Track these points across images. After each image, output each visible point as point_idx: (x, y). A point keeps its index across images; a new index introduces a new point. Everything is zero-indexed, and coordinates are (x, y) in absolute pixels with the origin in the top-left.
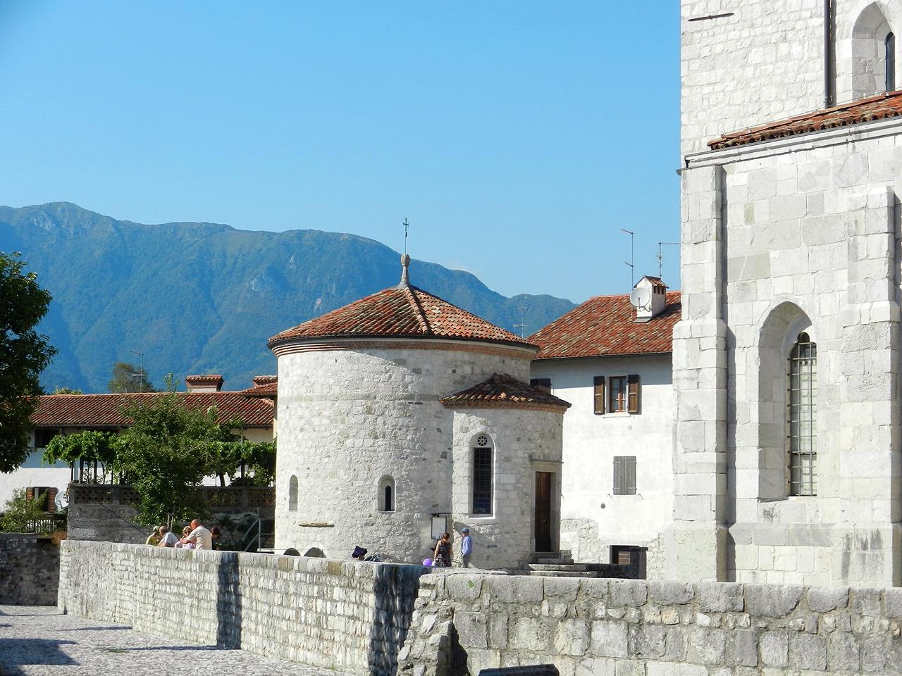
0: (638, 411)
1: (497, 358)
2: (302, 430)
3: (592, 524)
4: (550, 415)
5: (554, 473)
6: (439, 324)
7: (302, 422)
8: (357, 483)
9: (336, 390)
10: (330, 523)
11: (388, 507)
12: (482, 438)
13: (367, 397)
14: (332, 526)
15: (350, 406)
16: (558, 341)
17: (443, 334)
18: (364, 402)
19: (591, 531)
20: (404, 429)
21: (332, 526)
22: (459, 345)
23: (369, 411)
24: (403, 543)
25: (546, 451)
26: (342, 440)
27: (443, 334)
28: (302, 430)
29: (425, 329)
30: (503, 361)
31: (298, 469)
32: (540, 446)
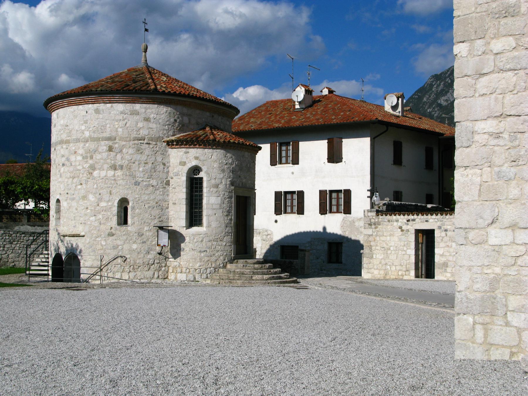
0: (297, 163)
1: (208, 114)
2: (63, 165)
3: (269, 233)
4: (247, 154)
5: (250, 197)
6: (164, 86)
7: (64, 159)
8: (103, 204)
9: (87, 134)
10: (82, 234)
11: (123, 220)
12: (196, 170)
13: (109, 139)
14: (84, 236)
15: (96, 146)
16: (248, 123)
17: (166, 91)
18: (106, 142)
19: (269, 237)
20: (137, 163)
21: (84, 236)
22: (179, 100)
23: (110, 149)
24: (136, 249)
25: (244, 180)
26: (91, 171)
27: (166, 91)
28: (63, 165)
29: (153, 87)
30: (213, 116)
31: (60, 194)
32: (240, 177)
